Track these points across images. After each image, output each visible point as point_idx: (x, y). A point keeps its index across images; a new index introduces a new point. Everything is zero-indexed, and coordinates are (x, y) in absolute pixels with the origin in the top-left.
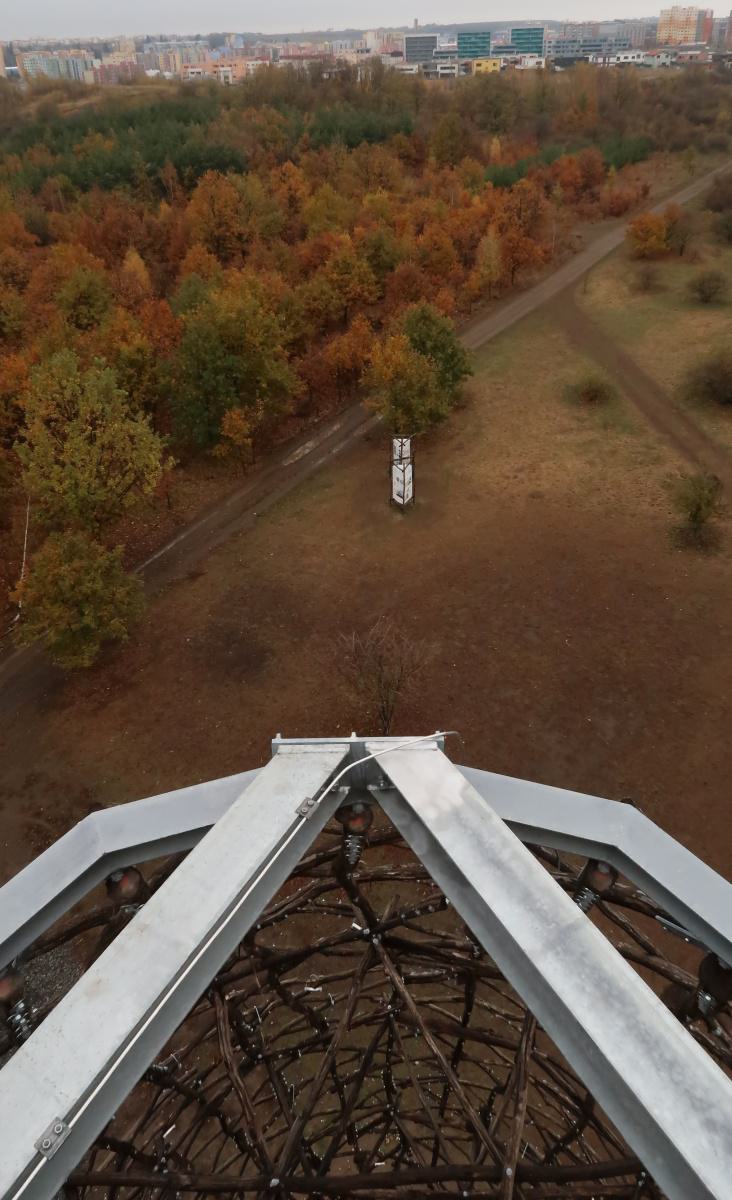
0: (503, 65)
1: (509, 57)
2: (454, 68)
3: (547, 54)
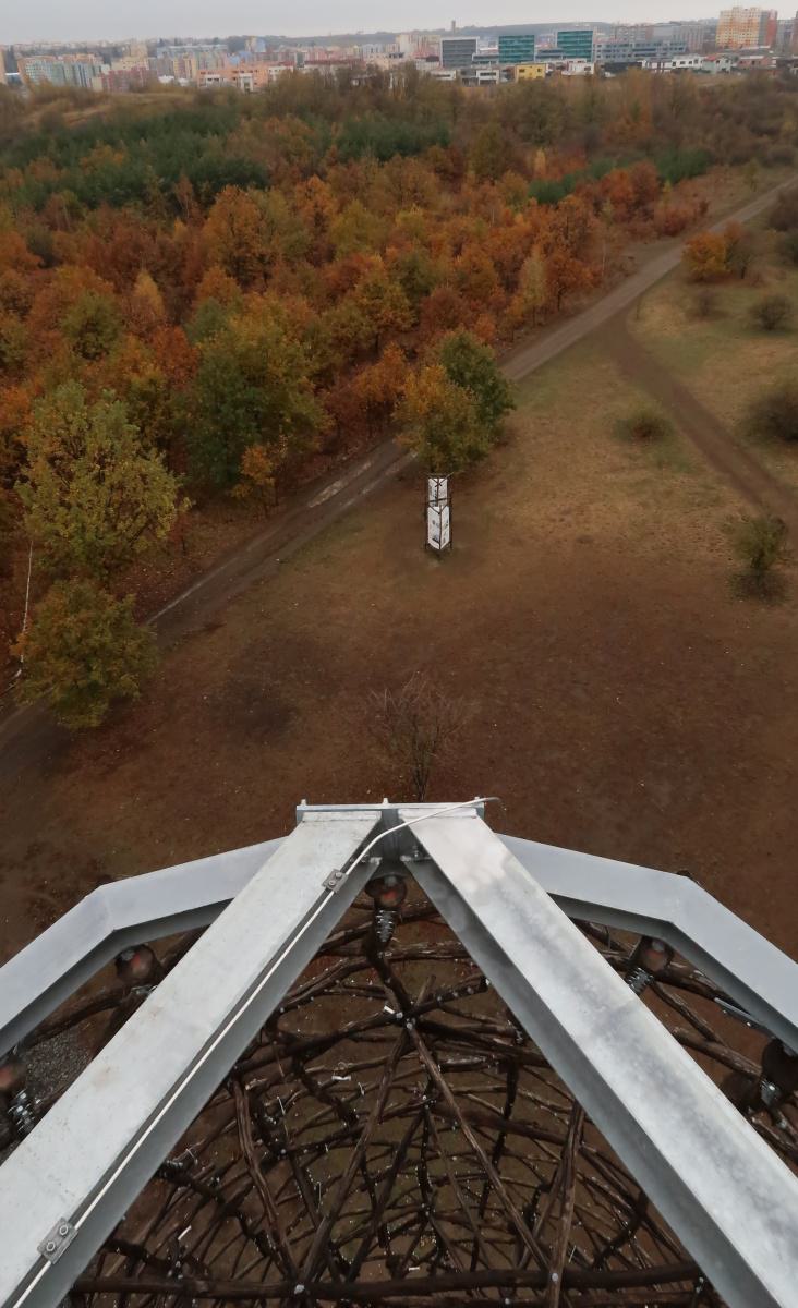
0: (548, 70)
1: (554, 62)
2: (495, 74)
3: (596, 59)
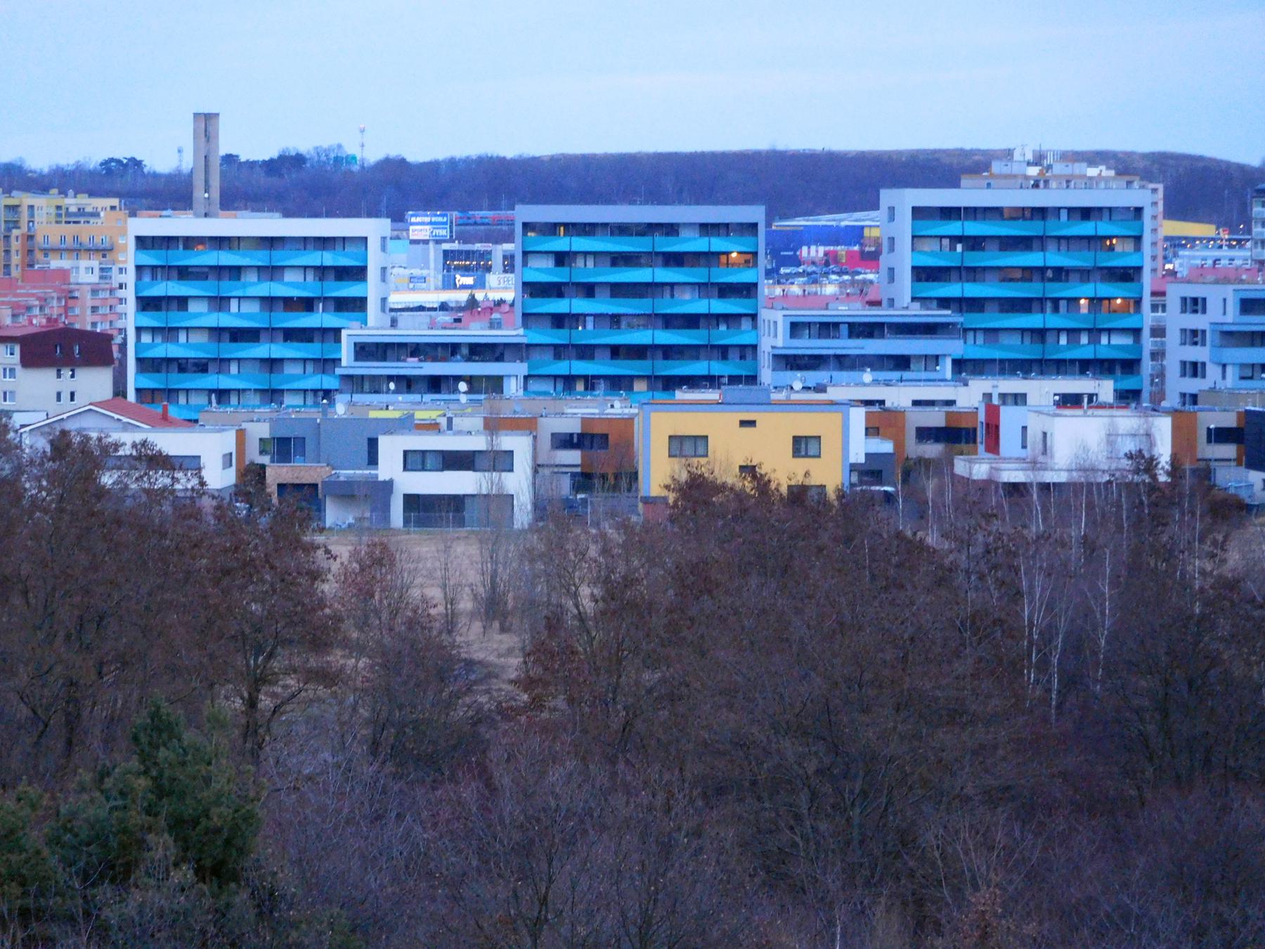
0: (860, 447)
1: (899, 396)
2: (502, 461)
3: (1177, 384)
